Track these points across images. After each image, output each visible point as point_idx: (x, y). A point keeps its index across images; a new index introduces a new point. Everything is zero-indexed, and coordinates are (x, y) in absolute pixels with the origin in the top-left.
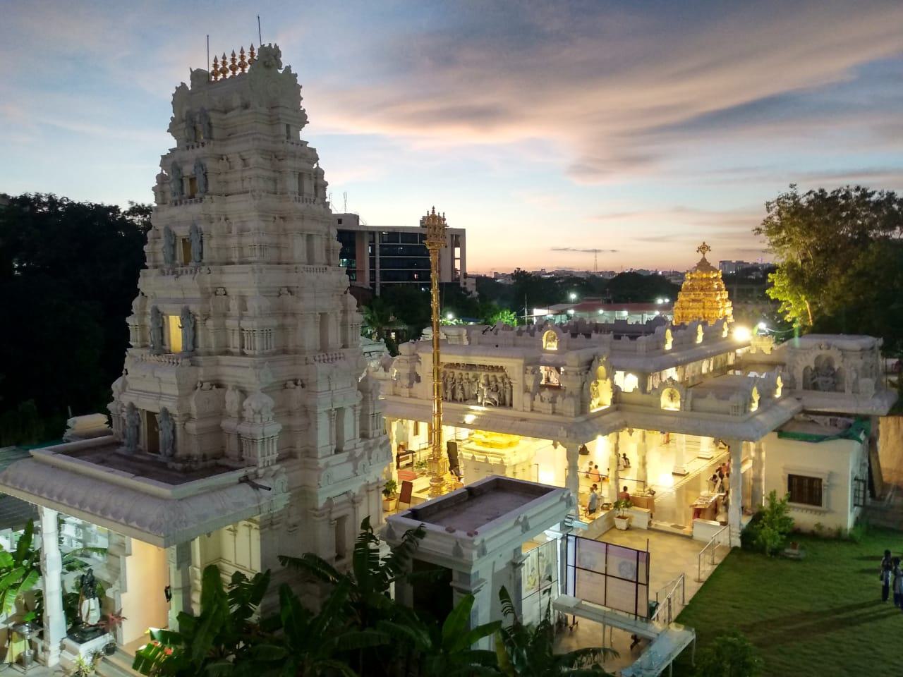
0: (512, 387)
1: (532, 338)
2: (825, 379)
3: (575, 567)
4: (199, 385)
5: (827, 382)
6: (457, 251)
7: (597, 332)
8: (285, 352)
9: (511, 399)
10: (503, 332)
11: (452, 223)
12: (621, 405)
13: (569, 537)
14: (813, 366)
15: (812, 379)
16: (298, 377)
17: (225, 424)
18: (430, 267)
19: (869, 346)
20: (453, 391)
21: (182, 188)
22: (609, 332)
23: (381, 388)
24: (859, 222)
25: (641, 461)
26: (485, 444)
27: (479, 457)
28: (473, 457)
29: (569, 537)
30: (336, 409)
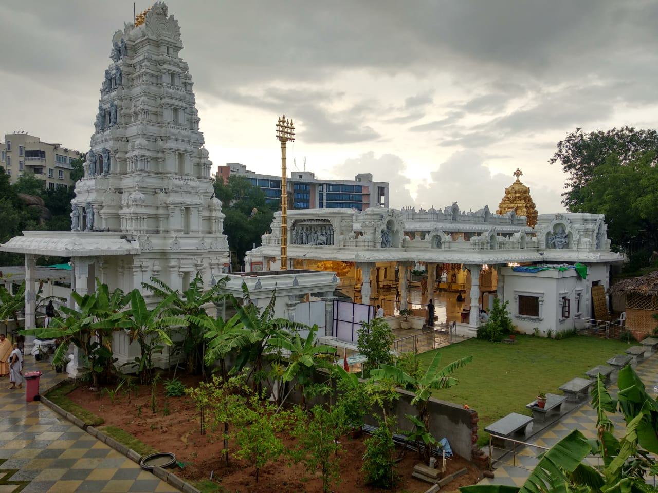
3: (337, 320)
5: (561, 242)
6: (382, 198)
14: (552, 231)
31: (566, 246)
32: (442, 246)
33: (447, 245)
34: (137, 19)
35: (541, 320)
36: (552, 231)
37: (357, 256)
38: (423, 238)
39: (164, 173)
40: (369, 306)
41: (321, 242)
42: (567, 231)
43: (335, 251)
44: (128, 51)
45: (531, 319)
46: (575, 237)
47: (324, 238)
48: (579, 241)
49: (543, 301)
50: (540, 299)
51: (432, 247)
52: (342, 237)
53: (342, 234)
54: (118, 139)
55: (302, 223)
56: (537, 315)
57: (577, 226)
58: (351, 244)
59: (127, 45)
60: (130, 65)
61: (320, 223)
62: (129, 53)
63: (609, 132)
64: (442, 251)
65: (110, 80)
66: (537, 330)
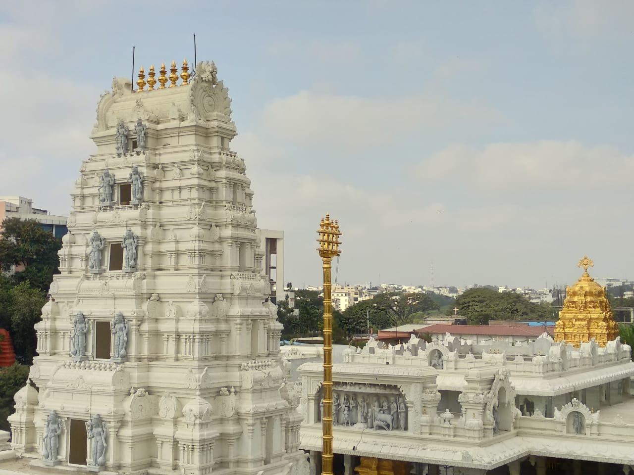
0: (407, 408)
4: (132, 391)
8: (216, 358)
16: (230, 384)
17: (158, 431)
21: (112, 195)
30: (266, 418)
32: (587, 431)
33: (595, 430)
34: (142, 76)
37: (466, 457)
38: (549, 414)
39: (228, 358)
41: (382, 424)
43: (415, 443)
44: (149, 139)
47: (388, 418)
51: (568, 432)
53: (424, 412)
54: (141, 297)
55: (340, 389)
58: (446, 432)
59: (149, 131)
60: (156, 166)
62: (150, 142)
64: (587, 439)
65: (112, 187)
66: (474, 440)
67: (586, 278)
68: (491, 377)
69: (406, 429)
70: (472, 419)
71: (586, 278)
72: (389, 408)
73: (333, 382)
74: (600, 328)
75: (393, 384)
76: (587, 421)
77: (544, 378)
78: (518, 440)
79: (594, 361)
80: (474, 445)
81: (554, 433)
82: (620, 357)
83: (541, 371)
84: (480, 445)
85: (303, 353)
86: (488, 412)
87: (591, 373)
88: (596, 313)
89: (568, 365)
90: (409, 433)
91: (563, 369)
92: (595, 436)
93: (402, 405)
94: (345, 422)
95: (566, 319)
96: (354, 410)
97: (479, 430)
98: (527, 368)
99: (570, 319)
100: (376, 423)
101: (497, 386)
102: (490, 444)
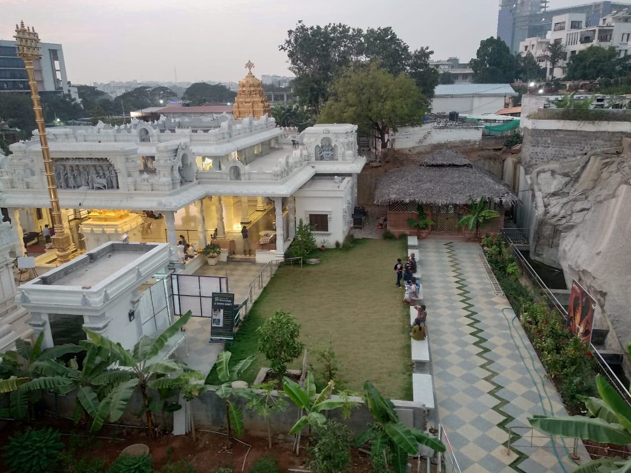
0: (116, 173)
1: (129, 134)
2: (327, 152)
3: (179, 295)
5: (328, 155)
6: (57, 63)
7: (179, 127)
9: (118, 183)
10: (105, 131)
11: (46, 37)
12: (201, 180)
13: (173, 276)
14: (320, 145)
15: (320, 154)
18: (27, 78)
19: (350, 131)
20: (66, 180)
22: (188, 128)
23: (443, 204)
24: (342, 49)
25: (219, 217)
26: (100, 219)
27: (98, 230)
28: (92, 230)
29: (173, 276)
31: (333, 158)
32: (242, 178)
35: (330, 234)
36: (320, 145)
37: (160, 204)
40: (220, 278)
41: (99, 186)
42: (333, 145)
45: (321, 234)
46: (340, 151)
47: (104, 181)
48: (344, 154)
49: (330, 218)
50: (329, 216)
51: (231, 179)
52: (130, 179)
53: (129, 175)
56: (326, 230)
57: (342, 140)
58: (146, 188)
61: (94, 163)
63: (326, 27)
67: (580, 152)
68: (176, 147)
69: (118, 187)
70: (163, 179)
71: (580, 152)
72: (104, 174)
73: (52, 159)
74: (259, 107)
75: (104, 157)
76: (242, 172)
77: (217, 144)
78: (199, 187)
79: (251, 130)
80: (166, 195)
81: (221, 180)
82: (268, 126)
83: (215, 139)
84: (170, 195)
85: (54, 133)
86: (175, 172)
87: (261, 134)
88: (257, 99)
89: (233, 134)
90: (120, 191)
91: (230, 137)
92: (248, 181)
93: (113, 172)
94: (73, 186)
95: (239, 102)
96: (78, 177)
97: (168, 185)
98: (206, 138)
99: (242, 103)
100: (95, 185)
101: (180, 154)
102: (178, 193)
